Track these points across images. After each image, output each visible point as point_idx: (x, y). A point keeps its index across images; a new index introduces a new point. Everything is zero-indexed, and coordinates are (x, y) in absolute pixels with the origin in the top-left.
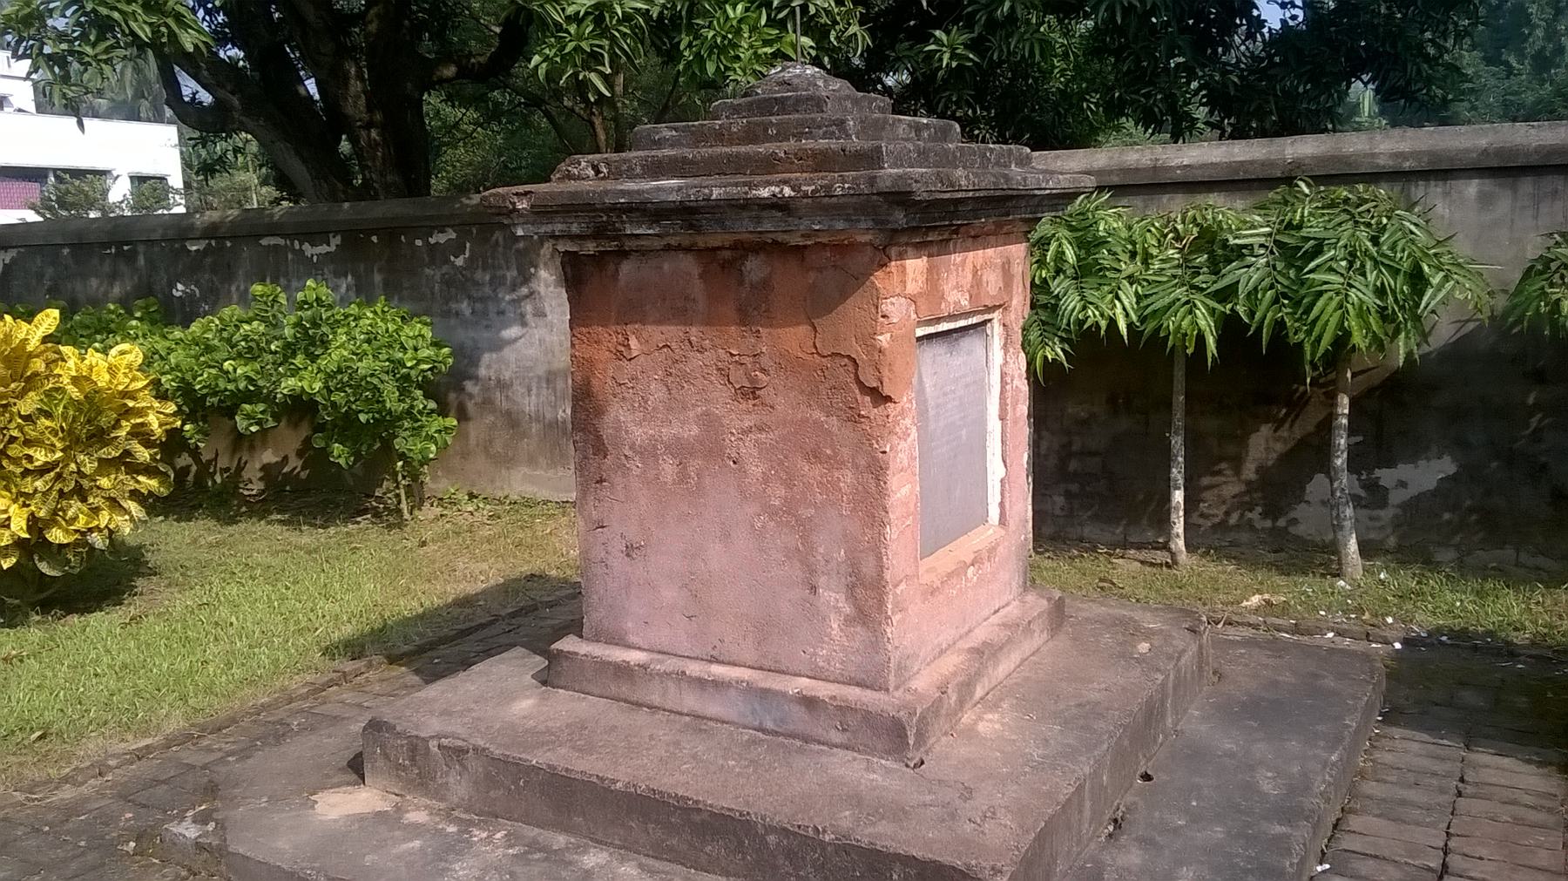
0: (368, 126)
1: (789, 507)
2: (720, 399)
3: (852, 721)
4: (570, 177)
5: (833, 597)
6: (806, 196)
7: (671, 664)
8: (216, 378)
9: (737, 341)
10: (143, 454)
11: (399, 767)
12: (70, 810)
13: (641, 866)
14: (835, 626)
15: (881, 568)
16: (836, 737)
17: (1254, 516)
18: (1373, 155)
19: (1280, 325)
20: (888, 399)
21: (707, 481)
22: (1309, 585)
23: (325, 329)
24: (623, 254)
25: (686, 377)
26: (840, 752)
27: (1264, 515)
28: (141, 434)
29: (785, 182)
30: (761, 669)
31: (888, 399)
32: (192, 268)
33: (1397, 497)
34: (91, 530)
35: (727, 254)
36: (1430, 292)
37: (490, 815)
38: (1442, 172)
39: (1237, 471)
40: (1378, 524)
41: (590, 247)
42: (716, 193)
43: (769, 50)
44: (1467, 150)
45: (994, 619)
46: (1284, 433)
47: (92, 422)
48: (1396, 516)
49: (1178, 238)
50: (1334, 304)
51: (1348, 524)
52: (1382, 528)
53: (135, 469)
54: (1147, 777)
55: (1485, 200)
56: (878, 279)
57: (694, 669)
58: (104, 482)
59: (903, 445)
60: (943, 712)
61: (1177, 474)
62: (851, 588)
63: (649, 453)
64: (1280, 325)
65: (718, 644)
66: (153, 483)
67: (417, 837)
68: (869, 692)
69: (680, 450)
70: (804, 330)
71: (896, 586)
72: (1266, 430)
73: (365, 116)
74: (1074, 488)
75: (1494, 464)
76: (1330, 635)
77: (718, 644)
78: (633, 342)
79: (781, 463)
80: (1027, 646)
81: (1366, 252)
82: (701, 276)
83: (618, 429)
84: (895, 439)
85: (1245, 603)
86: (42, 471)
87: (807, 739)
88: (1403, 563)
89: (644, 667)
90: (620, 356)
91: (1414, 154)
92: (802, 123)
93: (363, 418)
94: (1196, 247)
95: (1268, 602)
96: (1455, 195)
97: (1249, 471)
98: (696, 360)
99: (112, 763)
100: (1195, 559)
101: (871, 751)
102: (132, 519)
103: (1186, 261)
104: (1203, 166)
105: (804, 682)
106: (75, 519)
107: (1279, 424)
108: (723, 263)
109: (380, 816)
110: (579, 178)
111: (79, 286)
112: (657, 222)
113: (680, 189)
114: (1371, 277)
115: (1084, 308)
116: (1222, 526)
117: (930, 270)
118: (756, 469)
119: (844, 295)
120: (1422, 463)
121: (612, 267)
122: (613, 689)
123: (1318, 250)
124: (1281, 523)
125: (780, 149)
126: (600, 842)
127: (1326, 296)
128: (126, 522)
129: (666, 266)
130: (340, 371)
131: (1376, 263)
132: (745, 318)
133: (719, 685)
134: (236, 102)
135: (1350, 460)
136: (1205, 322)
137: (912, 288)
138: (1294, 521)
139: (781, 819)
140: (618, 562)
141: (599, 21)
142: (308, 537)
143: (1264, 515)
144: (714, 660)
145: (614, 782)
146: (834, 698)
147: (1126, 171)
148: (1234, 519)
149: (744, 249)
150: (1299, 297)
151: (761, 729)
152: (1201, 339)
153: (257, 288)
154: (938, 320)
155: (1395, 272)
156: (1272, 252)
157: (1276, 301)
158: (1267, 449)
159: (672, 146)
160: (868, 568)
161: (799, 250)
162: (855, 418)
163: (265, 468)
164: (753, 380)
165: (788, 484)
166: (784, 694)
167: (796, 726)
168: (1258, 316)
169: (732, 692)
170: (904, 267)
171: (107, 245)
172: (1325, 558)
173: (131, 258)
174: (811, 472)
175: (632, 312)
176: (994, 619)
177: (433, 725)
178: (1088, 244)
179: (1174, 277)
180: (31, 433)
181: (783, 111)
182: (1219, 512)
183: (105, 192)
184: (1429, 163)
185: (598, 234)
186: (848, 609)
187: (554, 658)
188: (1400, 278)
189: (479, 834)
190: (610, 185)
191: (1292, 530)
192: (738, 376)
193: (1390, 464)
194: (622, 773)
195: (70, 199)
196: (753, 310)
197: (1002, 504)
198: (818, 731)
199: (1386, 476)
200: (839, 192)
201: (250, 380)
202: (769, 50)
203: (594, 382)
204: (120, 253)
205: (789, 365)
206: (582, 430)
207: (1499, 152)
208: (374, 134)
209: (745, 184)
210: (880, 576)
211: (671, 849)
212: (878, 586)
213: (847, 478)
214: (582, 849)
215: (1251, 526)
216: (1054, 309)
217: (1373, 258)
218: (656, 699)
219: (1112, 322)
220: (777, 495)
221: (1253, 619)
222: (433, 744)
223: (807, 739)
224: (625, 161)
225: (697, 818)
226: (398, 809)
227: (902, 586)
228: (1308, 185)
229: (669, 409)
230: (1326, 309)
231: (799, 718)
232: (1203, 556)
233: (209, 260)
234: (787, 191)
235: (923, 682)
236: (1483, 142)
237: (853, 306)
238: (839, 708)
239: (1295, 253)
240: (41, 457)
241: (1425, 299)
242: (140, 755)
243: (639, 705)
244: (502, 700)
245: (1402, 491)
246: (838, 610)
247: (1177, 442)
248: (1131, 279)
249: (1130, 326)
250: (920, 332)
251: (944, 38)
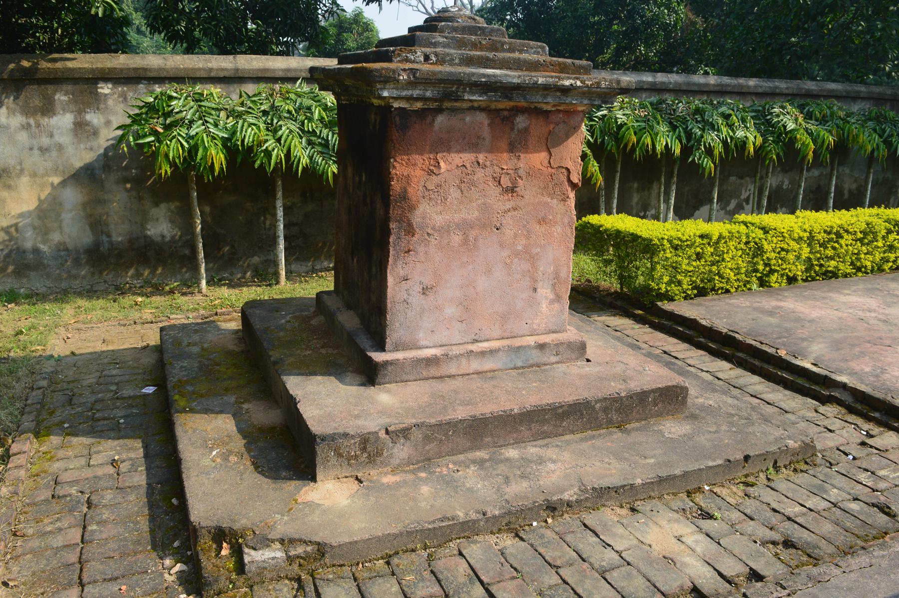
1: (527, 250)
4: (407, 60)
6: (587, 86)
9: (507, 161)
14: (544, 306)
21: (481, 241)
25: (473, 184)
29: (577, 79)
30: (503, 338)
35: (506, 113)
42: (541, 81)
62: (554, 285)
63: (445, 230)
65: (478, 332)
68: (560, 335)
69: (465, 227)
77: (478, 332)
78: (442, 164)
79: (525, 226)
82: (489, 125)
98: (480, 173)
108: (502, 119)
110: (414, 62)
112: (486, 93)
113: (519, 77)
121: (430, 118)
126: (502, 446)
129: (468, 119)
132: (512, 148)
133: (492, 352)
140: (416, 299)
144: (476, 341)
145: (511, 410)
159: (444, 47)
161: (547, 112)
165: (528, 237)
166: (529, 346)
169: (501, 353)
190: (438, 68)
192: (506, 182)
196: (517, 145)
198: (545, 360)
200: (603, 86)
203: (410, 190)
206: (398, 221)
209: (556, 77)
218: (453, 371)
225: (560, 411)
231: (536, 356)
234: (579, 83)
243: (441, 377)
246: (546, 298)
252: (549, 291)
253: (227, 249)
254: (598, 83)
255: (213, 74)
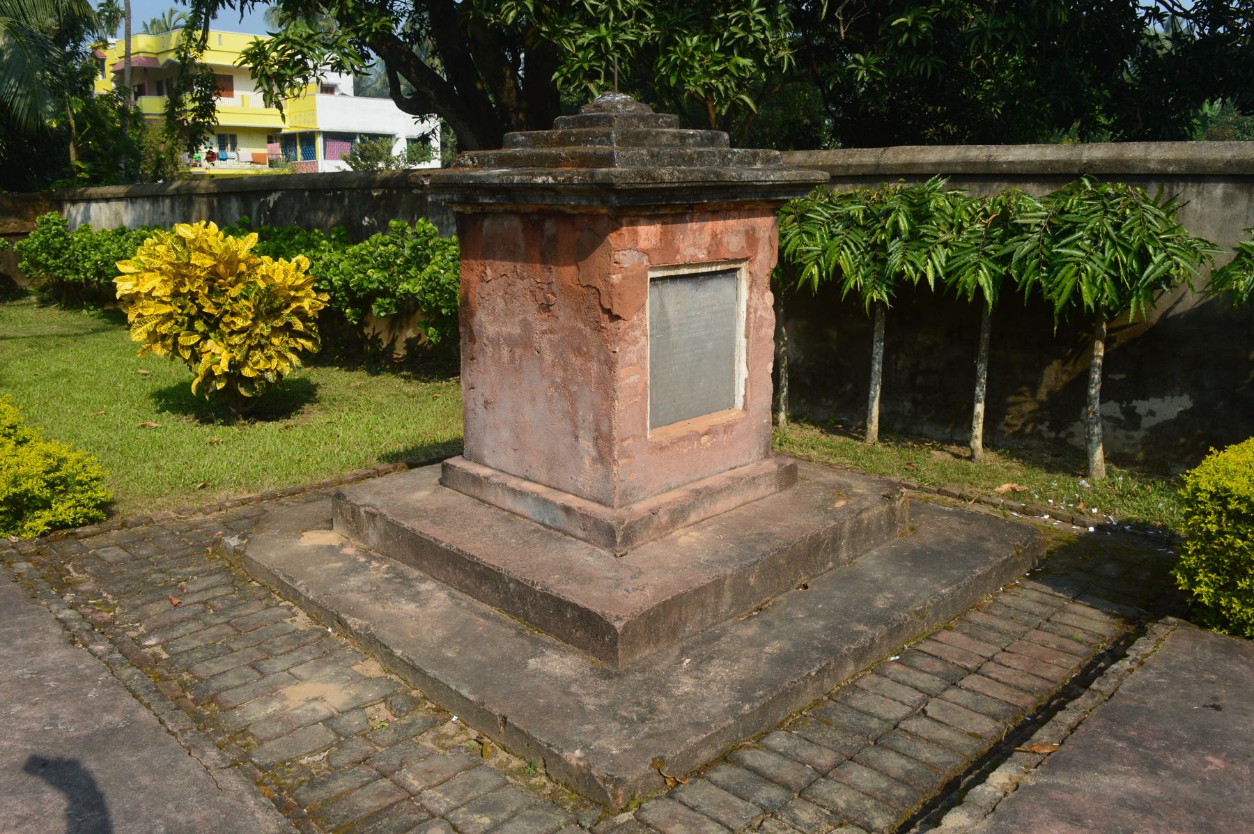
0: (517, 111)
1: (565, 385)
2: (532, 314)
3: (589, 524)
5: (586, 444)
7: (502, 478)
8: (362, 279)
10: (299, 326)
11: (347, 521)
12: (195, 526)
13: (449, 594)
15: (611, 427)
16: (581, 534)
17: (1043, 427)
18: (1146, 161)
19: (1037, 285)
20: (618, 317)
21: (524, 363)
22: (1057, 481)
23: (428, 252)
24: (484, 215)
26: (581, 543)
27: (1051, 428)
28: (299, 313)
29: (549, 174)
31: (618, 317)
32: (373, 207)
33: (1147, 422)
34: (267, 370)
35: (535, 217)
36: (1151, 267)
37: (386, 555)
38: (1198, 175)
39: (1034, 394)
40: (1132, 442)
41: (469, 210)
43: (718, 68)
44: (1216, 161)
45: (729, 473)
46: (1069, 368)
47: (271, 305)
48: (1146, 437)
49: (986, 216)
50: (1073, 272)
51: (1095, 439)
52: (1134, 445)
53: (296, 334)
54: (805, 587)
55: (1228, 199)
56: (612, 239)
57: (513, 483)
58: (275, 341)
59: (631, 348)
60: (653, 526)
61: (980, 392)
62: (596, 439)
63: (495, 343)
64: (1037, 285)
66: (309, 345)
67: (342, 560)
68: (602, 508)
69: (512, 342)
70: (573, 269)
71: (623, 440)
72: (1056, 364)
73: (515, 104)
74: (919, 396)
75: (1221, 404)
76: (1047, 517)
78: (489, 271)
80: (750, 494)
81: (1107, 235)
83: (481, 326)
84: (622, 343)
85: (998, 489)
86: (242, 331)
87: (566, 533)
88: (1149, 474)
89: (487, 478)
90: (482, 279)
91: (1177, 162)
92: (588, 134)
93: (444, 311)
94: (996, 223)
95: (1014, 490)
96: (1206, 195)
97: (1042, 394)
98: (520, 285)
99: (228, 504)
100: (991, 455)
101: (597, 544)
102: (291, 365)
103: (987, 232)
104: (1022, 163)
105: (570, 497)
106: (258, 362)
107: (1066, 361)
108: (533, 222)
109: (331, 548)
111: (312, 217)
114: (1108, 254)
115: (903, 264)
116: (1020, 434)
117: (664, 233)
118: (548, 357)
119: (594, 247)
120: (1168, 398)
122: (472, 491)
123: (1070, 232)
124: (1062, 435)
125: (563, 151)
127: (1068, 266)
128: (290, 367)
130: (430, 279)
131: (1114, 244)
133: (522, 494)
134: (432, 94)
135: (1102, 391)
136: (984, 279)
137: (643, 244)
138: (1071, 435)
139: (517, 575)
140: (480, 410)
141: (598, 49)
142: (414, 387)
143: (1051, 428)
144: (527, 479)
146: (580, 508)
147: (967, 163)
148: (1028, 429)
149: (546, 214)
150: (1052, 264)
151: (543, 524)
152: (979, 289)
153: (393, 223)
154: (677, 267)
155: (1127, 251)
156: (1045, 230)
157: (1038, 267)
158: (1057, 379)
160: (604, 428)
161: (572, 216)
162: (599, 329)
163: (408, 341)
164: (547, 299)
167: (562, 524)
168: (1024, 278)
170: (636, 233)
171: (328, 191)
172: (1077, 464)
173: (340, 199)
174: (576, 361)
175: (488, 253)
176: (729, 473)
177: (368, 499)
178: (920, 215)
179: (977, 245)
180: (236, 307)
181: (591, 125)
182: (1019, 423)
183: (390, 149)
184: (1187, 168)
185: (466, 201)
186: (594, 453)
187: (445, 468)
188: (1130, 256)
189: (375, 564)
191: (1070, 441)
193: (1145, 397)
194: (446, 537)
195: (367, 153)
196: (548, 256)
197: (745, 397)
198: (571, 529)
199: (1141, 406)
201: (381, 283)
202: (718, 68)
203: (470, 296)
204: (335, 194)
205: (567, 291)
207: (1240, 163)
208: (521, 116)
210: (611, 432)
211: (467, 586)
212: (609, 439)
213: (594, 367)
214: (423, 580)
215: (1039, 435)
216: (884, 262)
217: (1112, 239)
218: (492, 499)
219: (924, 276)
220: (559, 375)
221: (996, 501)
222: (362, 509)
223: (566, 533)
224: (486, 156)
225: (478, 569)
226: (342, 545)
227: (630, 441)
228: (1091, 181)
229: (506, 315)
230: (1066, 277)
232: (1000, 454)
233: (383, 203)
234: (551, 180)
235: (640, 507)
236: (1228, 155)
237: (598, 255)
238: (582, 515)
239: (1059, 230)
240: (240, 323)
241: (1147, 272)
242: (243, 503)
243: (484, 502)
244: (419, 492)
245: (1151, 418)
247: (982, 368)
248: (946, 244)
249: (937, 279)
250: (651, 274)
251: (862, 59)
252: (591, 444)
253: (849, 386)
254: (571, 178)
255: (851, 172)
